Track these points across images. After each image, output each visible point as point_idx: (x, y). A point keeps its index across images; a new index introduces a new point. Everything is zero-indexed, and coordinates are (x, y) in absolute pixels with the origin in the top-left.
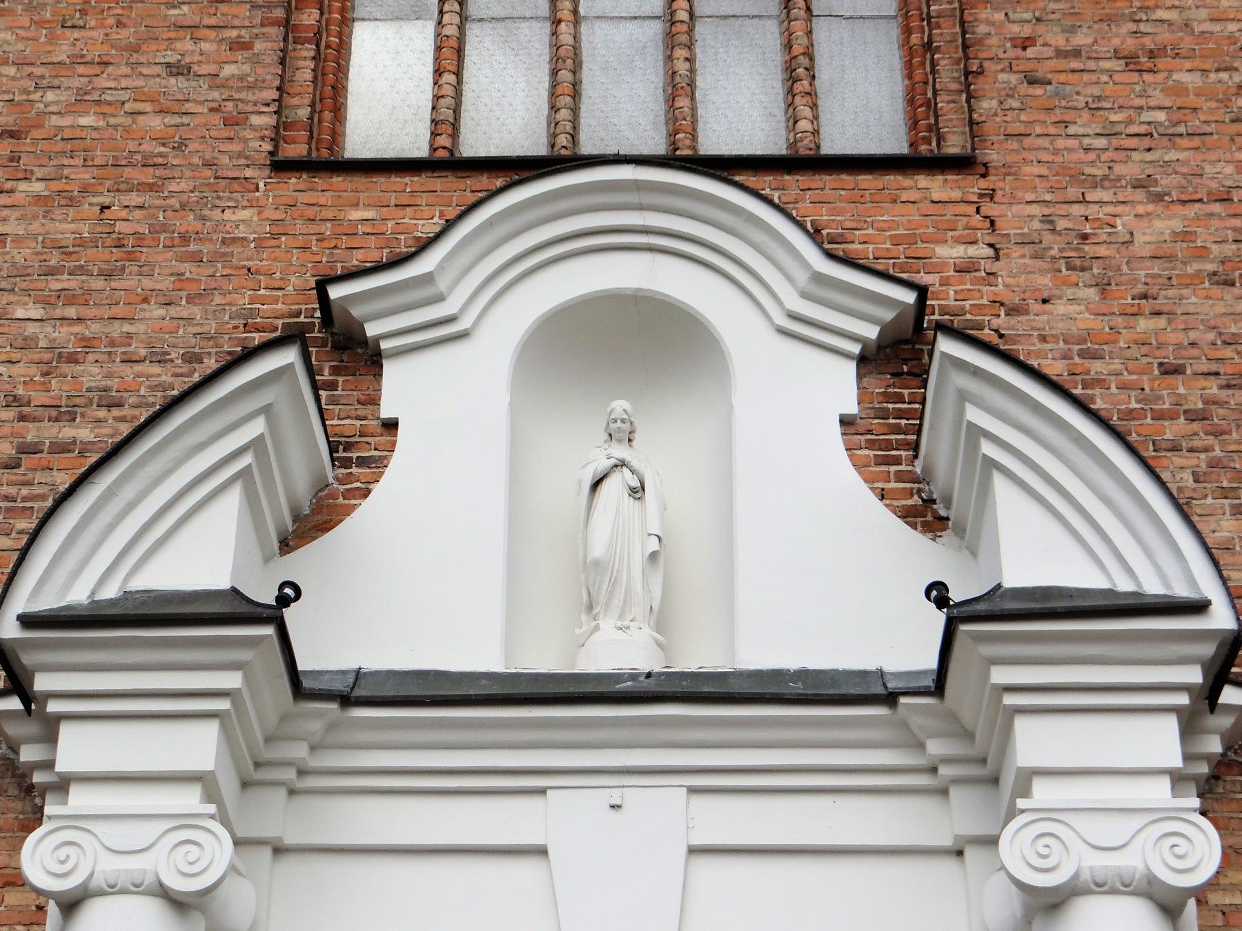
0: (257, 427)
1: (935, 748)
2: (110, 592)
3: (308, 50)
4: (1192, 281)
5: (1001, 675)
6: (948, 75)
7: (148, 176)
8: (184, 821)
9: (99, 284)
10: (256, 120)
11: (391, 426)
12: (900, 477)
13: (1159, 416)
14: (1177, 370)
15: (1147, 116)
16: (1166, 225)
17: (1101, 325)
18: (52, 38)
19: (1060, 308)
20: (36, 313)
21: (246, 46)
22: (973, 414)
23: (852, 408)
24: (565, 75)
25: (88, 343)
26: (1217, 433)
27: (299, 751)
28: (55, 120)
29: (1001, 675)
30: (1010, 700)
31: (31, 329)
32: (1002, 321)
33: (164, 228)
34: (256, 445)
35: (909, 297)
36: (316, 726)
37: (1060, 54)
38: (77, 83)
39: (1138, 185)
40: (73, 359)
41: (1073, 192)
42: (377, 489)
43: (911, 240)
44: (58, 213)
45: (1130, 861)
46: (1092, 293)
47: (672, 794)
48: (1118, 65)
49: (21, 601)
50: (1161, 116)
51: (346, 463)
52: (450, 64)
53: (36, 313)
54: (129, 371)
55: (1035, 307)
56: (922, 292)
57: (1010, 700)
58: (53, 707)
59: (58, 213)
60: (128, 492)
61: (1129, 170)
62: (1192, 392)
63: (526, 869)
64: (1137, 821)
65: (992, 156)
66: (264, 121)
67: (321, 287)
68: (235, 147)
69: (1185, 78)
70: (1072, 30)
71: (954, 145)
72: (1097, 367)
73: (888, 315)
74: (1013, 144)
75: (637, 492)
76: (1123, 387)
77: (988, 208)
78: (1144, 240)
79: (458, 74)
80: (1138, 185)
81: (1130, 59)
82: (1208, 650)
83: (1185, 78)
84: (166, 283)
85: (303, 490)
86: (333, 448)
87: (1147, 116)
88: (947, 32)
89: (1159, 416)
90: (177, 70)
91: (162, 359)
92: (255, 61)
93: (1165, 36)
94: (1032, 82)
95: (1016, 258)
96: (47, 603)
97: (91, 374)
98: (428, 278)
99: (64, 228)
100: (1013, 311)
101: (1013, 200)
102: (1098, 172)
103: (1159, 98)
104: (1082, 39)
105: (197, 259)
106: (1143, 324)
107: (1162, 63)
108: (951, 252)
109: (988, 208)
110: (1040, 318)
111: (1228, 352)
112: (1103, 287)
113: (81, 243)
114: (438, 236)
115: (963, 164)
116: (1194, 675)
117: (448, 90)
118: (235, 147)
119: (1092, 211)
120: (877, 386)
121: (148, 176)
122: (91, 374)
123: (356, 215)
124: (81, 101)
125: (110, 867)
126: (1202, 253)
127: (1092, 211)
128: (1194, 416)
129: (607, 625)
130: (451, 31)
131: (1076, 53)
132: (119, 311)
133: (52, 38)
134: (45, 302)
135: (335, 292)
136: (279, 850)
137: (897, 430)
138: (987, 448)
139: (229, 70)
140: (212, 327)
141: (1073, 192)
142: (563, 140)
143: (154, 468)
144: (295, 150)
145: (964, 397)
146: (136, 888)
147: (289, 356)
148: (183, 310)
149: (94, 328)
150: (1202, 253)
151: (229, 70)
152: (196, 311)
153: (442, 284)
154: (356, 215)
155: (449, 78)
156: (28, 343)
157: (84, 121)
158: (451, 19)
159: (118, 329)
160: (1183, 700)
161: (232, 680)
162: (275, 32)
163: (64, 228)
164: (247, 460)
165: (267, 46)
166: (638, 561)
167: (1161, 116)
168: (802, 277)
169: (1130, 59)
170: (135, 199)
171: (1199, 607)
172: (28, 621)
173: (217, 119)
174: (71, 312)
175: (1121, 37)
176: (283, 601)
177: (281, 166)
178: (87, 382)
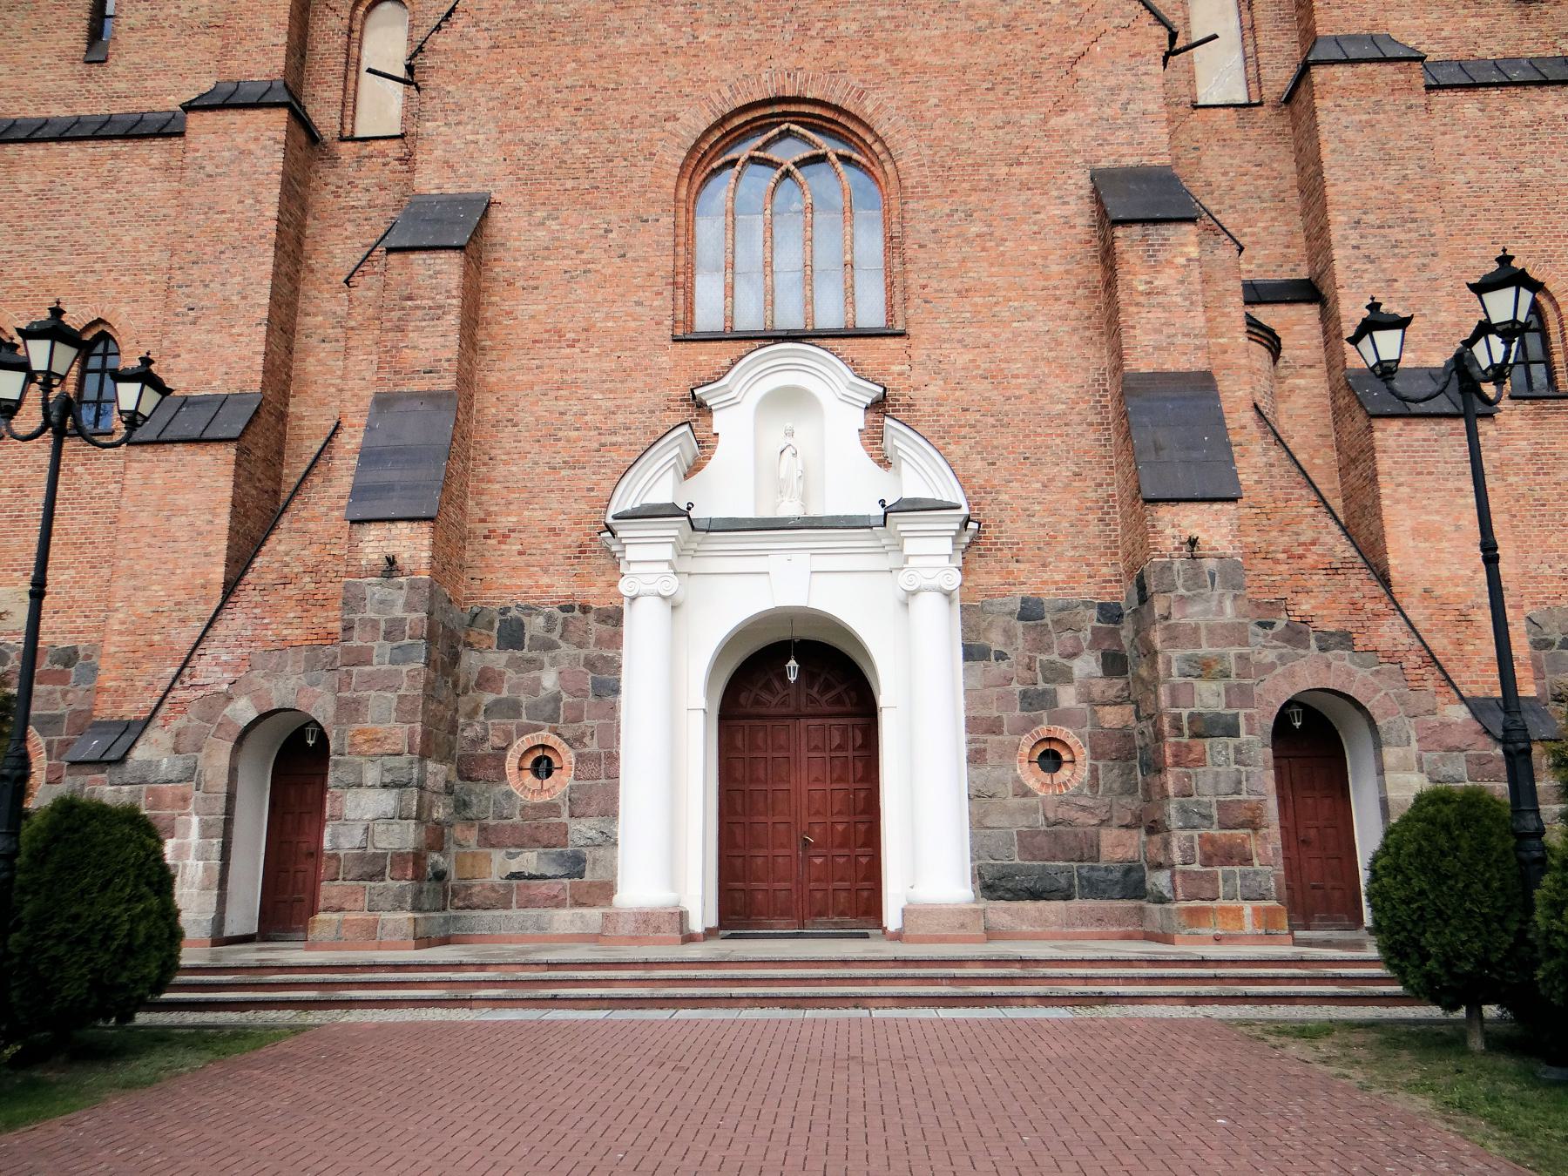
0: (677, 450)
1: (884, 542)
2: (637, 505)
3: (681, 292)
4: (974, 377)
5: (900, 527)
6: (898, 297)
7: (632, 345)
8: (664, 574)
9: (619, 385)
10: (666, 323)
11: (717, 434)
12: (877, 449)
13: (960, 426)
14: (967, 410)
15: (963, 315)
16: (968, 357)
17: (944, 394)
18: (596, 292)
19: (931, 388)
20: (600, 396)
21: (661, 294)
22: (896, 442)
23: (862, 426)
24: (769, 297)
25: (618, 407)
26: (978, 432)
27: (694, 546)
28: (599, 324)
29: (900, 527)
30: (903, 534)
31: (600, 402)
32: (911, 393)
33: (639, 364)
34: (677, 456)
35: (881, 390)
36: (699, 539)
37: (936, 291)
38: (605, 309)
39: (960, 341)
40: (614, 413)
41: (937, 345)
42: (714, 457)
43: (883, 363)
44: (604, 360)
45: (935, 582)
46: (941, 382)
47: (805, 556)
48: (955, 295)
49: (612, 511)
50: (968, 315)
51: (703, 448)
52: (729, 293)
53: (600, 396)
54: (632, 416)
55: (923, 387)
56: (885, 389)
57: (903, 534)
58: (624, 541)
59: (604, 360)
60: (640, 474)
61: (957, 336)
62: (971, 417)
63: (764, 577)
64: (938, 570)
65: (910, 331)
66: (669, 322)
67: (692, 390)
68: (660, 333)
69: (977, 299)
70: (940, 281)
71: (899, 328)
72: (942, 409)
73: (874, 395)
74: (918, 327)
75: (795, 455)
76: (950, 416)
77: (909, 351)
78: (960, 362)
79: (732, 297)
80: (960, 341)
81: (959, 292)
82: (961, 519)
83: (977, 299)
84: (641, 385)
85: (690, 458)
86: (698, 443)
87: (963, 315)
88: (898, 281)
89: (960, 426)
90: (639, 303)
91: (642, 412)
92: (664, 299)
93: (972, 283)
94: (926, 302)
95: (918, 370)
96: (620, 510)
97: (620, 418)
98: (726, 386)
99: (607, 365)
100: (916, 389)
101: (917, 348)
102: (946, 337)
103: (968, 308)
104: (944, 285)
105: (650, 375)
106: (958, 393)
107: (970, 294)
108: (896, 368)
109: (909, 351)
110: (924, 392)
111: (984, 403)
112: (945, 380)
113: (612, 371)
114: (730, 368)
115: (901, 335)
116: (957, 527)
117: (729, 304)
118: (660, 333)
119: (943, 352)
120: (871, 416)
121: (632, 345)
122: (620, 418)
123: (701, 358)
124: (607, 317)
125: (644, 589)
126: (978, 367)
127: (943, 352)
128: (973, 426)
129: (786, 499)
130: (729, 280)
131: (942, 290)
132: (627, 395)
133: (596, 292)
134: (602, 392)
135: (697, 392)
136: (690, 574)
137: (876, 433)
138: (900, 453)
139: (656, 303)
140: (657, 400)
141: (937, 345)
142: (768, 323)
143: (649, 463)
144: (679, 332)
145: (893, 436)
146: (652, 595)
147: (686, 428)
148: (648, 394)
149: (619, 402)
150: (978, 367)
151: (656, 303)
152: (651, 395)
153: (730, 387)
154: (701, 358)
155: (729, 299)
156: (599, 408)
157: (610, 324)
158: (729, 276)
159: (628, 402)
160: (953, 533)
161: (675, 533)
162: (671, 287)
163: (607, 365)
164: (674, 461)
165: (668, 293)
166: (795, 478)
167: (968, 315)
168: (847, 383)
169: (959, 292)
170: (628, 353)
171: (958, 507)
172: (615, 517)
173: (653, 322)
174: (612, 396)
175: (957, 284)
176: (689, 509)
177: (676, 340)
178: (619, 421)
